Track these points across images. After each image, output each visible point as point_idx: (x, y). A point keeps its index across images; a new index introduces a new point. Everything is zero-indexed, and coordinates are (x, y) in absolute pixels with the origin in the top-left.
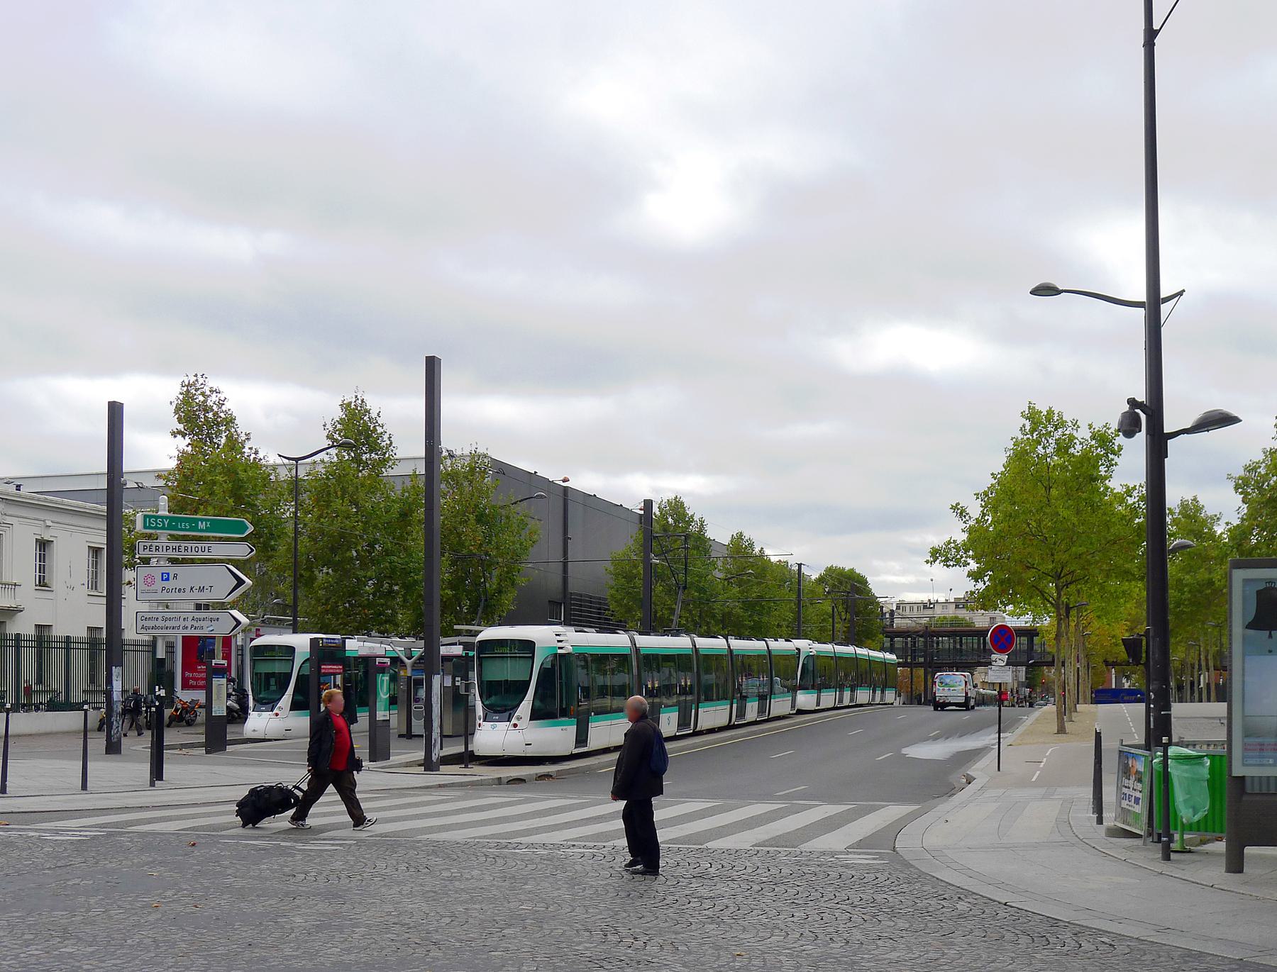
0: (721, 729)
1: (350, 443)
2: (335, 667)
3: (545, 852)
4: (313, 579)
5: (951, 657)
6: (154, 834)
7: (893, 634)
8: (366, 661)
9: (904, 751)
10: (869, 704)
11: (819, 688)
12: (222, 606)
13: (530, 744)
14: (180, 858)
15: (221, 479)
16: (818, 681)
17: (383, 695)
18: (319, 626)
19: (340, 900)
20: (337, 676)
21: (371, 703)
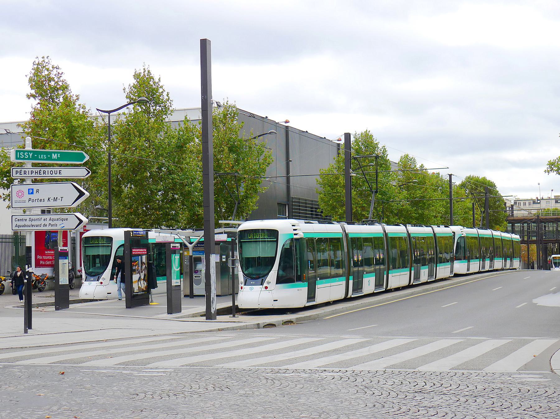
0: (404, 288)
1: (144, 100)
2: (142, 250)
3: (307, 375)
4: (121, 191)
5: (555, 236)
6: (34, 366)
7: (513, 222)
8: (162, 247)
9: (535, 301)
10: (502, 269)
11: (468, 259)
12: (69, 210)
13: (277, 300)
14: (56, 383)
15: (61, 126)
16: (468, 254)
17: (175, 268)
18: (126, 223)
19: (174, 411)
21: (168, 273)
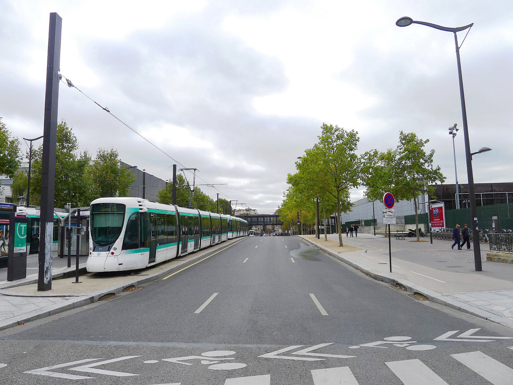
13: (122, 264)
20: (18, 225)
